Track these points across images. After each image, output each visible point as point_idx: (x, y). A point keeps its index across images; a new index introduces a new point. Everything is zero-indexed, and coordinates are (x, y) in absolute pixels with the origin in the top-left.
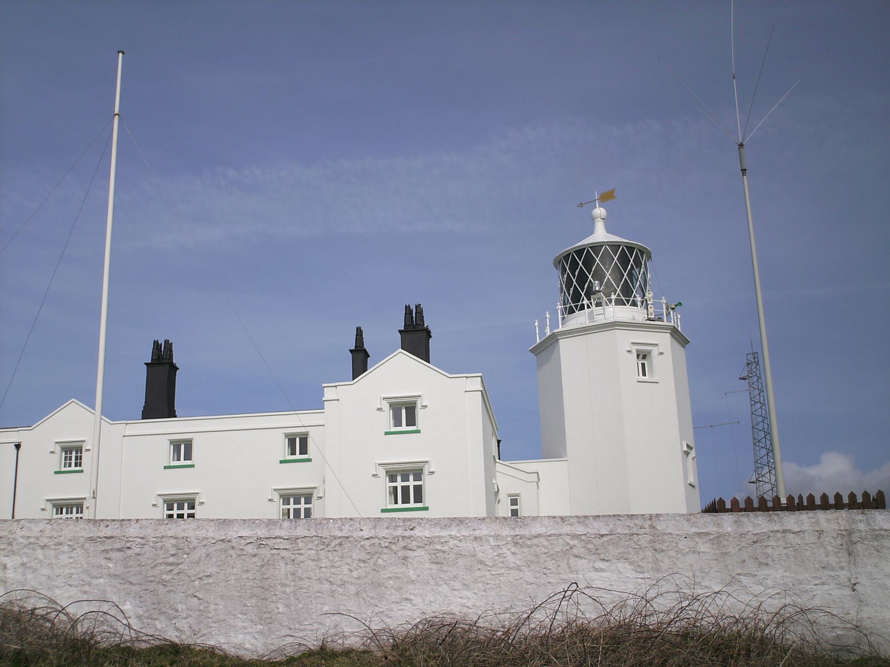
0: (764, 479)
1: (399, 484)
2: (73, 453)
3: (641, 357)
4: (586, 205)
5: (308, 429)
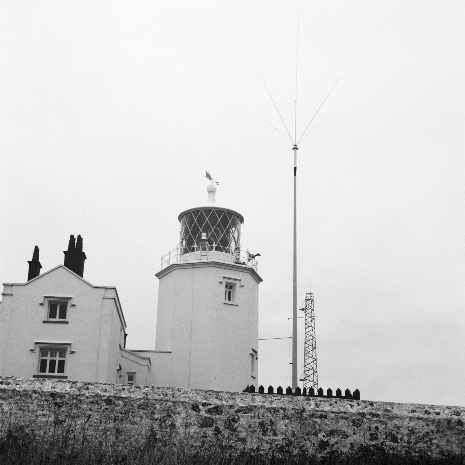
0: (309, 378)
3: (229, 287)
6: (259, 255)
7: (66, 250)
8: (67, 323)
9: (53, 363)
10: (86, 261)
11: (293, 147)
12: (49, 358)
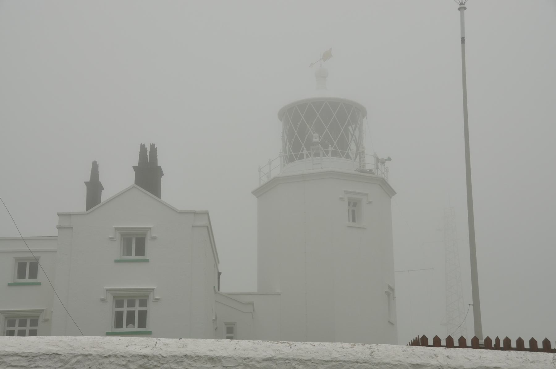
5: (36, 255)
6: (389, 159)
7: (136, 164)
8: (147, 261)
9: (131, 315)
10: (163, 178)
11: (459, 6)
12: (125, 309)
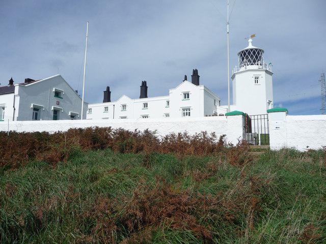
1: (185, 112)
2: (124, 106)
4: (247, 39)
